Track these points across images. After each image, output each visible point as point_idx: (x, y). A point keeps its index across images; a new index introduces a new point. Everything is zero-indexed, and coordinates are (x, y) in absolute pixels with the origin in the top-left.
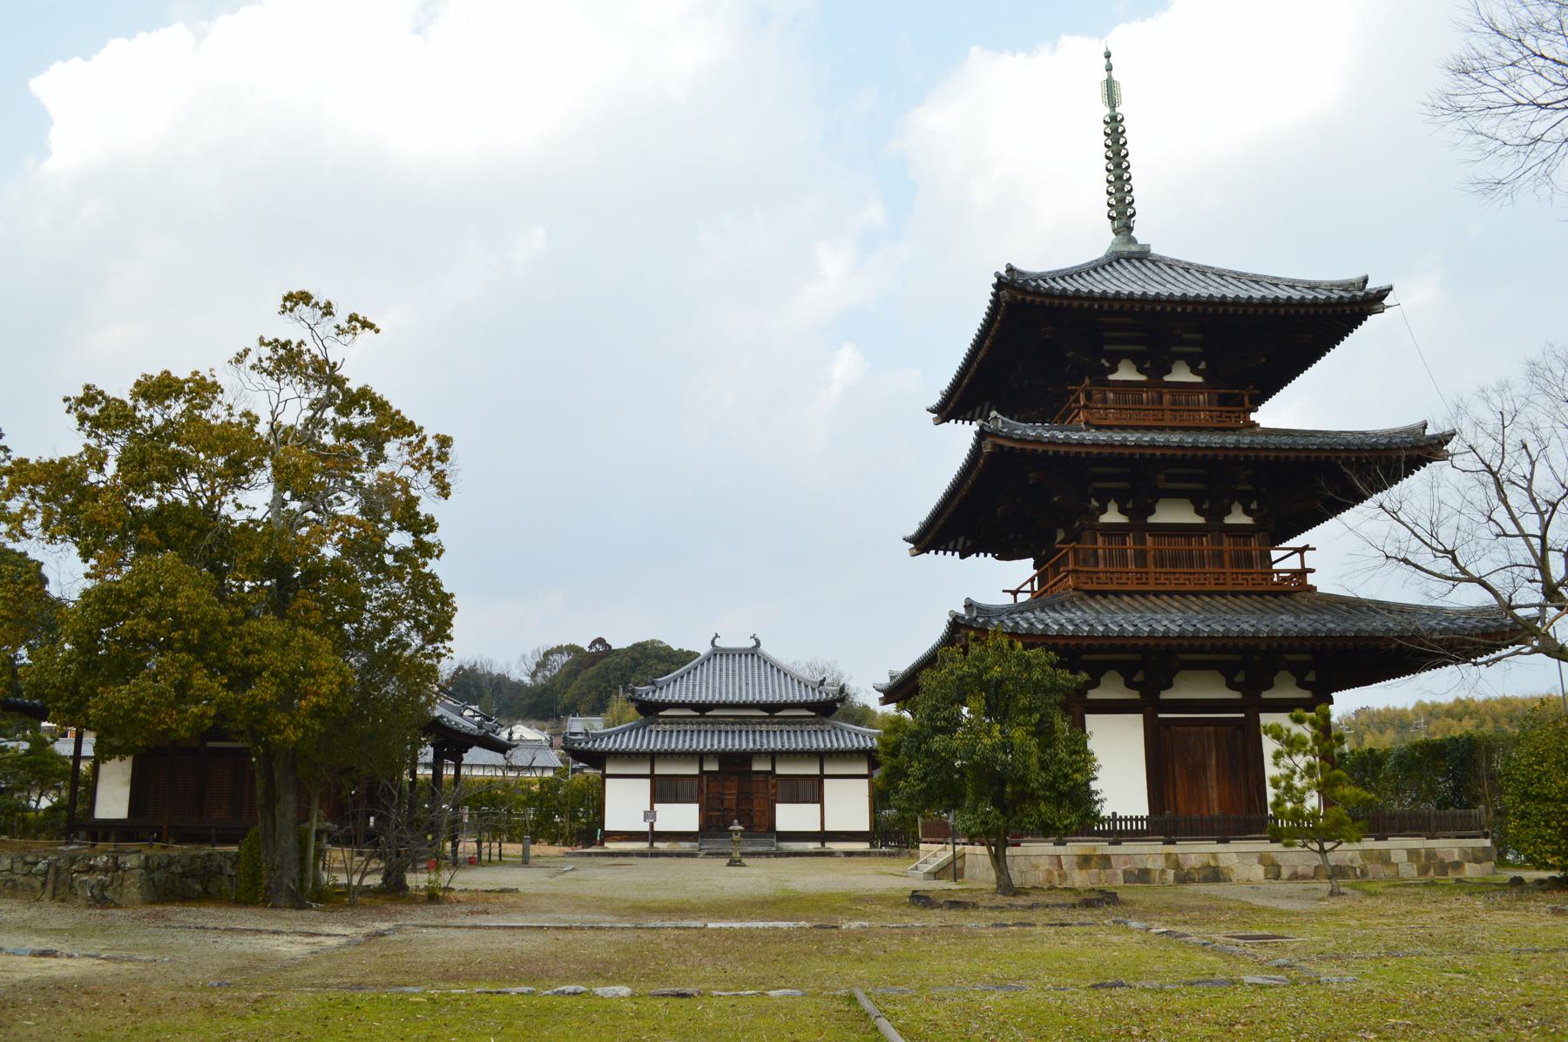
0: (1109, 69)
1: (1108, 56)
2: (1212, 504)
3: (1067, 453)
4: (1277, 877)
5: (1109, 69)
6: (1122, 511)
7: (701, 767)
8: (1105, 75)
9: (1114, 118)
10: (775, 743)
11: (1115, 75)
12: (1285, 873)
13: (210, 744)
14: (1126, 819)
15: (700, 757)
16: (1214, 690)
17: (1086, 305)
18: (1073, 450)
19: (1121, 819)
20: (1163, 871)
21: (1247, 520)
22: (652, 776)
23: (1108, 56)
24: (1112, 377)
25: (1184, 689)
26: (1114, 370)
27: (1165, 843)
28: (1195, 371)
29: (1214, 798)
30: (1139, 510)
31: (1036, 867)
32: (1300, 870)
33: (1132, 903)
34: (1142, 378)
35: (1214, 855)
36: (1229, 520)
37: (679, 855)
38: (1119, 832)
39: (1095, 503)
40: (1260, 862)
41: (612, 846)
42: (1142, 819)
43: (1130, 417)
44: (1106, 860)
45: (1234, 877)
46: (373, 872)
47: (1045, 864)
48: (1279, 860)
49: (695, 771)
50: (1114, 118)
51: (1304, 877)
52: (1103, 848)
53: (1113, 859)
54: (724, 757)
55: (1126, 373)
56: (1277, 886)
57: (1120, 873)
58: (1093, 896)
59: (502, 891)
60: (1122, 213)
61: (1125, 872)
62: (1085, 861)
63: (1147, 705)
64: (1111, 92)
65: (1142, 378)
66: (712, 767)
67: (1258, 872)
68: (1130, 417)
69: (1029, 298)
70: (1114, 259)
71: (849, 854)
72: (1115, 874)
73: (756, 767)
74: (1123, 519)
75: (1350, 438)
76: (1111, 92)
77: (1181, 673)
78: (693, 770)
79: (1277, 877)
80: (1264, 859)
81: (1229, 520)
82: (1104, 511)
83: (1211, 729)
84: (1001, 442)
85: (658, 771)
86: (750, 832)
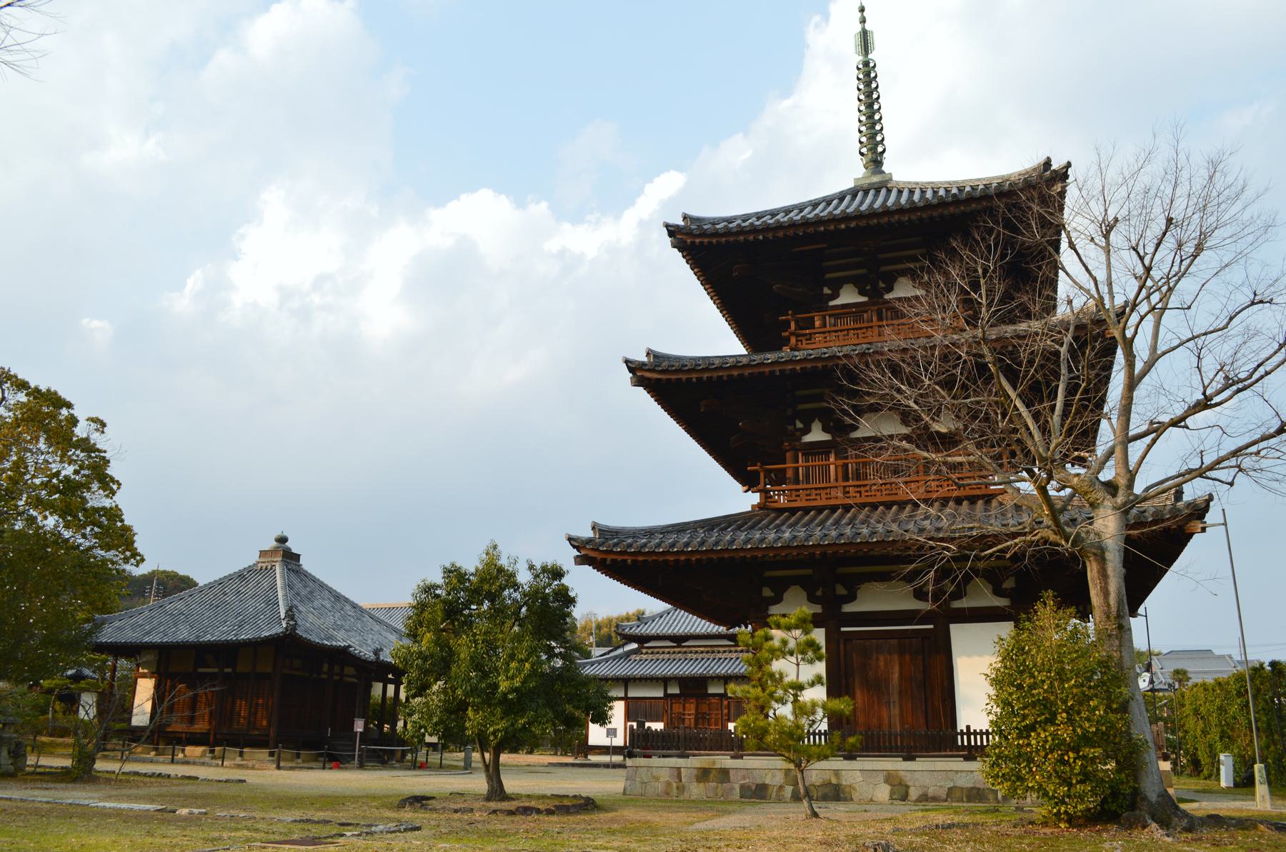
0: (863, 21)
1: (862, 10)
3: (710, 378)
4: (904, 797)
5: (863, 21)
6: (825, 430)
7: (665, 690)
8: (859, 28)
9: (866, 64)
10: (722, 670)
12: (914, 793)
13: (200, 670)
15: (665, 681)
17: (751, 238)
18: (715, 375)
20: (781, 787)
21: (826, 437)
22: (625, 699)
23: (862, 10)
24: (832, 303)
25: (872, 600)
26: (835, 296)
27: (905, 759)
29: (893, 715)
31: (657, 779)
32: (931, 792)
33: (384, 806)
34: (864, 299)
35: (837, 773)
36: (808, 438)
37: (567, 765)
39: (799, 425)
40: (887, 781)
41: (594, 758)
43: (883, 343)
44: (724, 773)
45: (855, 796)
47: (665, 776)
48: (908, 779)
49: (661, 694)
50: (866, 64)
51: (934, 799)
52: (724, 760)
53: (732, 773)
54: (683, 681)
55: (848, 297)
56: (900, 807)
57: (737, 787)
58: (702, 806)
59: (227, 781)
61: (742, 787)
62: (704, 775)
63: (829, 618)
64: (865, 41)
65: (864, 299)
66: (674, 690)
67: (883, 792)
68: (883, 343)
69: (697, 241)
71: (606, 766)
72: (733, 789)
73: (711, 690)
74: (826, 437)
76: (865, 41)
78: (659, 693)
79: (904, 797)
80: (890, 778)
81: (808, 438)
82: (807, 430)
83: (894, 642)
84: (648, 375)
85: (631, 694)
86: (560, 745)
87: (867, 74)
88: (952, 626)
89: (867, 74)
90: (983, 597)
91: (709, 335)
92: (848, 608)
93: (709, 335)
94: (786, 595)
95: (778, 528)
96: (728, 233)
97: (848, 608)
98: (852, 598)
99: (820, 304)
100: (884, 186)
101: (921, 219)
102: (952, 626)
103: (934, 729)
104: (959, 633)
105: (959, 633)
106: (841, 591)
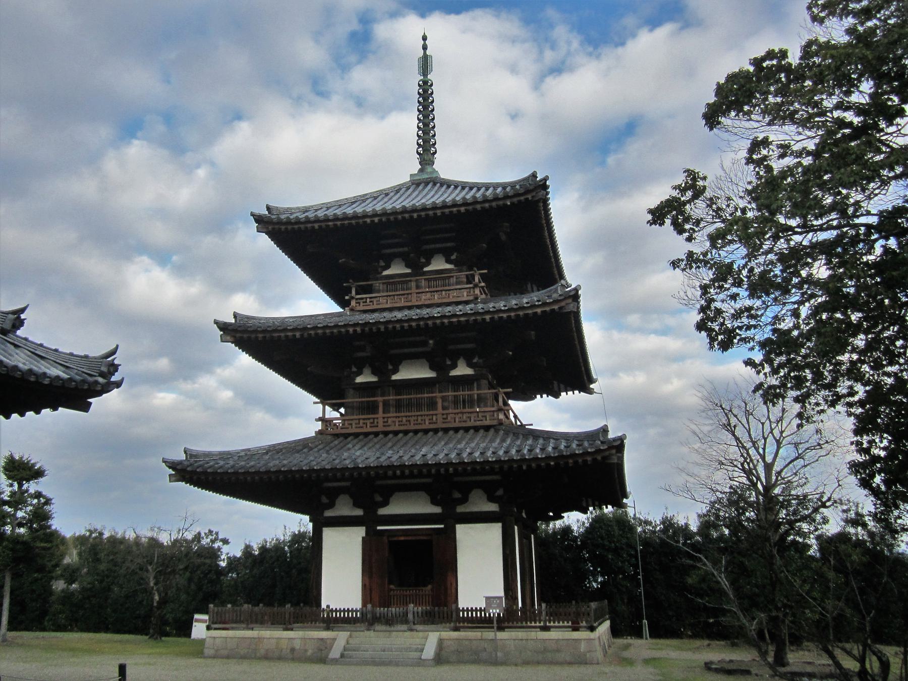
0: (425, 48)
2: (440, 361)
5: (425, 48)
9: (425, 83)
11: (428, 53)
14: (336, 611)
16: (421, 506)
19: (332, 611)
21: (469, 371)
23: (425, 38)
28: (448, 261)
30: (383, 371)
34: (409, 271)
36: (454, 373)
38: (335, 621)
42: (356, 611)
46: (757, 498)
50: (425, 83)
55: (397, 269)
60: (426, 149)
63: (369, 521)
70: (416, 183)
74: (469, 371)
75: (307, 321)
77: (397, 495)
81: (454, 373)
82: (454, 366)
87: (425, 91)
88: (324, 529)
89: (425, 91)
90: (344, 508)
91: (307, 301)
92: (382, 511)
93: (307, 301)
94: (337, 502)
95: (328, 452)
96: (288, 222)
97: (382, 511)
98: (385, 503)
99: (375, 273)
100: (437, 182)
101: (520, 201)
102: (324, 529)
103: (441, 606)
104: (463, 532)
105: (463, 532)
106: (457, 495)
